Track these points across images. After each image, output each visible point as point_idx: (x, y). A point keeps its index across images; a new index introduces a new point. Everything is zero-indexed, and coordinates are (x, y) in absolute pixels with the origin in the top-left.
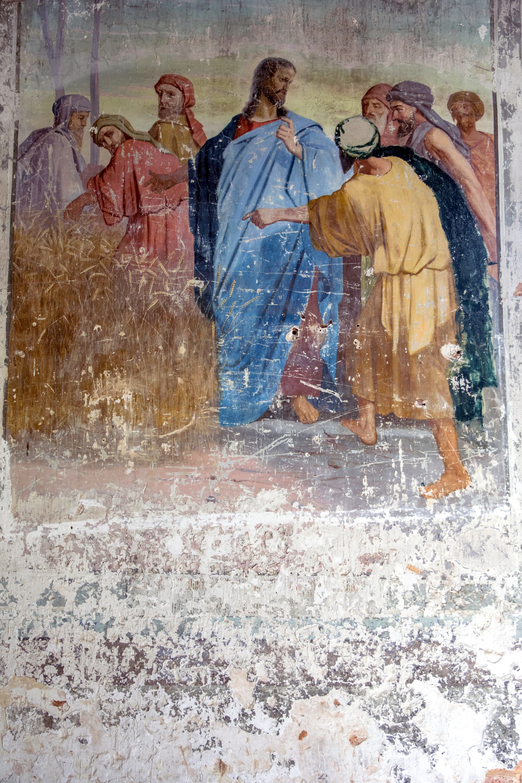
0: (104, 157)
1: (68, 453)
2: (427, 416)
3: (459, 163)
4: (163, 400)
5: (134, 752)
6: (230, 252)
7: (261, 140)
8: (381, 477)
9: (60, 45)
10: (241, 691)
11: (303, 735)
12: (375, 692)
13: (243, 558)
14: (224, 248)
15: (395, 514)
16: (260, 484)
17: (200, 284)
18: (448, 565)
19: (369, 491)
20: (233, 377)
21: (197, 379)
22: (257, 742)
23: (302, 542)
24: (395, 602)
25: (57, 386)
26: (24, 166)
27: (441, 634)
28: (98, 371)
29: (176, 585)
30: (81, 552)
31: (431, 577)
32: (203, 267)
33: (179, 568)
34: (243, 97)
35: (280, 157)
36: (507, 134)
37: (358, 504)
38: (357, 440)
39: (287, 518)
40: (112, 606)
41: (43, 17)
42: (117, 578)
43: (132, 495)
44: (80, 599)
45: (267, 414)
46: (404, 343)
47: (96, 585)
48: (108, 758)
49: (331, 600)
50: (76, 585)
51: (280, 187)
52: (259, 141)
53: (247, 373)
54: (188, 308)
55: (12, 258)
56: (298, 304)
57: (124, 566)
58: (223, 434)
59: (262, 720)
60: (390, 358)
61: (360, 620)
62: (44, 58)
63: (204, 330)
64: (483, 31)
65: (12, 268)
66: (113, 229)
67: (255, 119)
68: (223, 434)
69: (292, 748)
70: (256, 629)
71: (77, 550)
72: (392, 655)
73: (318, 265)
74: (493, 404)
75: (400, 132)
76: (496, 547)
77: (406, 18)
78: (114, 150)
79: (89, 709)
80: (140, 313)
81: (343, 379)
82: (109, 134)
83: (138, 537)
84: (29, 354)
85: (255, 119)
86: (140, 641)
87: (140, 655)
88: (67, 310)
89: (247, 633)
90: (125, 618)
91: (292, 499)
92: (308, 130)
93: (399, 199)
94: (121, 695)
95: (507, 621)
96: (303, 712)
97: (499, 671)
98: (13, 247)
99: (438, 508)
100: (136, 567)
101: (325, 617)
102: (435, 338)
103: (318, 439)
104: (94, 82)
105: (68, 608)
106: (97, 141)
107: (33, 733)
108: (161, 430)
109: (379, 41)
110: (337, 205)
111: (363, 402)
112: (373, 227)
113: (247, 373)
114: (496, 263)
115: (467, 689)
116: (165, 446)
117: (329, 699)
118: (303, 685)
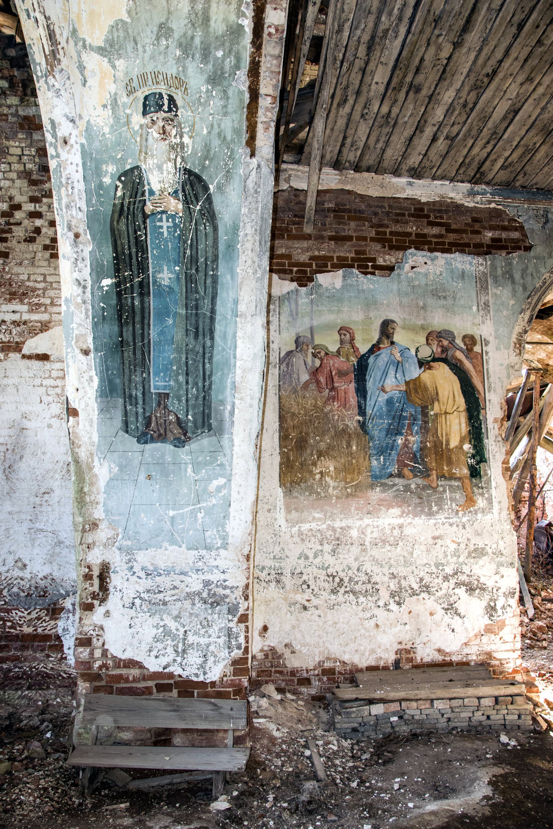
0: (318, 363)
1: (307, 494)
2: (458, 475)
3: (468, 365)
4: (347, 470)
5: (341, 620)
6: (373, 404)
7: (384, 356)
8: (440, 502)
9: (297, 314)
10: (384, 595)
11: (410, 612)
12: (440, 594)
13: (383, 538)
14: (370, 403)
15: (446, 518)
16: (389, 506)
17: (361, 418)
18: (468, 540)
19: (435, 508)
20: (376, 459)
21: (361, 460)
22: (391, 616)
23: (408, 531)
24: (447, 556)
25: (301, 464)
26: (283, 366)
27: (466, 569)
28: (319, 457)
29: (355, 550)
30: (315, 536)
31: (461, 545)
32: (362, 411)
33: (356, 543)
34: (376, 336)
35: (392, 362)
36: (487, 353)
37: (431, 514)
38: (429, 487)
39: (401, 521)
40: (329, 559)
41: (289, 302)
42: (331, 547)
43: (335, 511)
44: (315, 557)
45: (391, 475)
46: (448, 444)
47: (322, 551)
48: (330, 623)
49: (421, 556)
50: (313, 551)
51: (393, 375)
52: (383, 355)
53: (382, 458)
54: (356, 429)
55: (280, 408)
56: (403, 427)
57: (333, 542)
58: (373, 484)
59: (393, 606)
60: (442, 451)
61: (432, 564)
62: (290, 319)
63: (363, 439)
64: (475, 308)
65: (280, 412)
66: (323, 394)
67: (381, 346)
68: (373, 484)
69: (406, 618)
70: (389, 568)
71: (313, 535)
72: (446, 578)
73: (410, 410)
74: (485, 470)
75: (443, 351)
76: (488, 531)
77: (442, 302)
78: (321, 360)
79: (321, 603)
80: (336, 431)
81: (423, 460)
82: (319, 353)
83: (339, 530)
84: (289, 450)
85: (381, 346)
86: (341, 574)
87: (341, 580)
88: (304, 431)
89: (386, 570)
90: (336, 565)
91: (403, 512)
92: (404, 351)
93: (444, 380)
94: (334, 597)
95: (493, 563)
96: (410, 602)
97: (490, 584)
98: (280, 403)
99: (464, 515)
100: (338, 542)
101: (418, 563)
102: (461, 441)
103: (413, 486)
104: (312, 330)
105: (310, 560)
106: (314, 355)
107: (299, 612)
108: (347, 483)
109: (432, 312)
110: (418, 384)
111: (431, 470)
112: (433, 393)
113: (382, 458)
114: (485, 409)
115: (477, 591)
116: (349, 490)
117: (421, 597)
118: (410, 591)
